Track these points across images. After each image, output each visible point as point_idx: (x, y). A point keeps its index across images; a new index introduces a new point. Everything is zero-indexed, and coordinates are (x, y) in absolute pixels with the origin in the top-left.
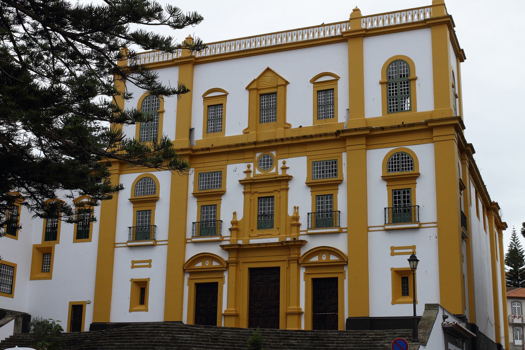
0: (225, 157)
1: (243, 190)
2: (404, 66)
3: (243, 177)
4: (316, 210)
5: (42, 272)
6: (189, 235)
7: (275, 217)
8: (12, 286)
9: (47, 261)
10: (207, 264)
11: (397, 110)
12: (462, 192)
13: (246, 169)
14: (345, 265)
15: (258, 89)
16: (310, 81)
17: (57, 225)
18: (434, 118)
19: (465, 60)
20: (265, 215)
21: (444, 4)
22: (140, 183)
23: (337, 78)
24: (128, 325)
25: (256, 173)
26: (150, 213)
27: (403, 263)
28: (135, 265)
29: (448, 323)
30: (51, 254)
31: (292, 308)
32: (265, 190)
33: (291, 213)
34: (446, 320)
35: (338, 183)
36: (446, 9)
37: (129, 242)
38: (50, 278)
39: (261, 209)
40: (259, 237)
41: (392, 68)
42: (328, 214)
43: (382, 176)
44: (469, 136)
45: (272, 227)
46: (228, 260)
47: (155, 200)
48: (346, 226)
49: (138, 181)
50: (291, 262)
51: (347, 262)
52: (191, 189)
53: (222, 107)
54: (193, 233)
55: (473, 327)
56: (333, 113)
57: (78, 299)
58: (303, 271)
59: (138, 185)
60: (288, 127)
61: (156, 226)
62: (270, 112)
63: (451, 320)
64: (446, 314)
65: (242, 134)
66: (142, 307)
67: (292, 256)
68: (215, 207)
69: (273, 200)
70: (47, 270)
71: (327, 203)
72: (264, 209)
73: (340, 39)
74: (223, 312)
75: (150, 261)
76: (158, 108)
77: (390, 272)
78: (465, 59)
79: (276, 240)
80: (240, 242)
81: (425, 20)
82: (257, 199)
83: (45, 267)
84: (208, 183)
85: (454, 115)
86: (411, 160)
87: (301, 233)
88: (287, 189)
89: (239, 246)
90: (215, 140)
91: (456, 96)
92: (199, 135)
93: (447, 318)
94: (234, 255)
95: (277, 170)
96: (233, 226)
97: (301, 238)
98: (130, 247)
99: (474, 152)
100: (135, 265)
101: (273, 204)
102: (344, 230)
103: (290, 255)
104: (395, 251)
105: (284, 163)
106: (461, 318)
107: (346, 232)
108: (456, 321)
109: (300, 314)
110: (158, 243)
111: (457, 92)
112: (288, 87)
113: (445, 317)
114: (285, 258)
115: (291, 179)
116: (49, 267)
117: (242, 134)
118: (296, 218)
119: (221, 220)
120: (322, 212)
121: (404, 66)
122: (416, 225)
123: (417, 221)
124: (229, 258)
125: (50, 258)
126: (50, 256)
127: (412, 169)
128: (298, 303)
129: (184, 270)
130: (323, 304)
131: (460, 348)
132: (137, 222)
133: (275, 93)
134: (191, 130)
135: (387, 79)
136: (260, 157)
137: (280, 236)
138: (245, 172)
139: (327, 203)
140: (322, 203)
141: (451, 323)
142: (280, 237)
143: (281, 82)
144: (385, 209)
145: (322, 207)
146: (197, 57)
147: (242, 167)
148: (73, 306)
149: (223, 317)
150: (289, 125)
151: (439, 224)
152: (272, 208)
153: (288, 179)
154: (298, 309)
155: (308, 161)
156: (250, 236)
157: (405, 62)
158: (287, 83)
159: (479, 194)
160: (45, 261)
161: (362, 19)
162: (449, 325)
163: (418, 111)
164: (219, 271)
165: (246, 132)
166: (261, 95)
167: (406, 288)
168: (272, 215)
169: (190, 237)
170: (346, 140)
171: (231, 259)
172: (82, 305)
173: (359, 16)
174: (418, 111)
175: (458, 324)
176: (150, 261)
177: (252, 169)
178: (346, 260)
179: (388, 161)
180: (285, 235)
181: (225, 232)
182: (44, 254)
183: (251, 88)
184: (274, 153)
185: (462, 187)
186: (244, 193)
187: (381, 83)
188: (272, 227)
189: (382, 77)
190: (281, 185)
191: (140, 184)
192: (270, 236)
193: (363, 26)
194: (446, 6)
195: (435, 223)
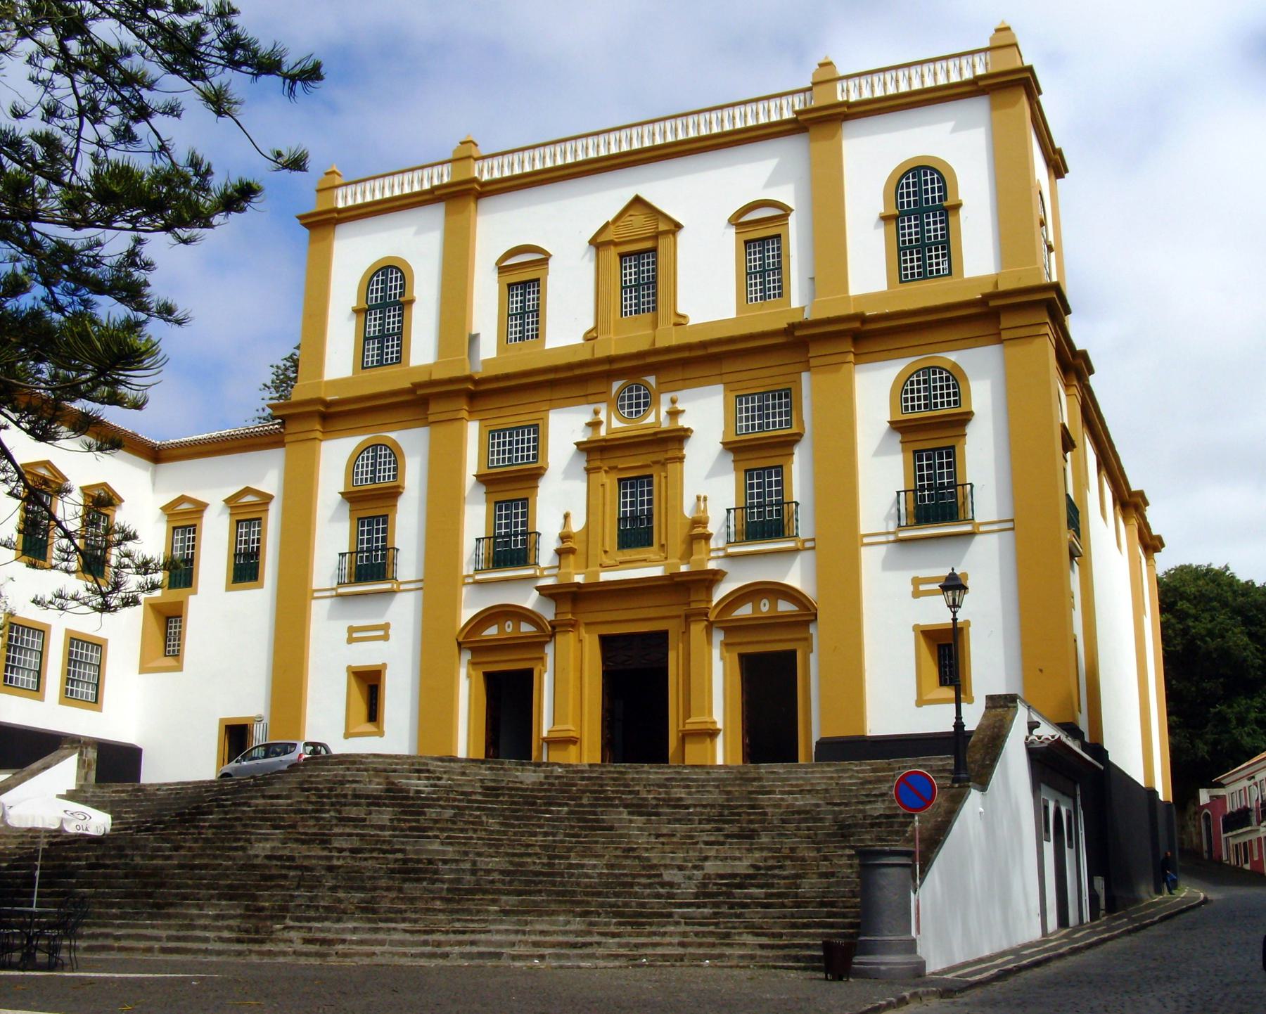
0: (546, 395)
1: (585, 465)
2: (932, 180)
3: (582, 438)
5: (165, 656)
6: (467, 568)
8: (97, 685)
9: (175, 633)
10: (509, 627)
11: (919, 274)
12: (1069, 454)
13: (588, 418)
14: (812, 621)
16: (730, 221)
17: (258, 547)
18: (1001, 288)
19: (1066, 175)
21: (1015, 45)
22: (363, 458)
23: (786, 211)
24: (354, 763)
25: (613, 426)
26: (385, 522)
27: (936, 612)
28: (355, 635)
29: (1039, 738)
30: (181, 616)
31: (695, 721)
32: (632, 463)
33: (688, 510)
34: (1036, 732)
35: (789, 443)
36: (1021, 57)
38: (179, 668)
39: (625, 506)
40: (621, 566)
41: (908, 184)
44: (1081, 333)
45: (650, 544)
46: (553, 618)
50: (692, 619)
52: (472, 464)
53: (538, 286)
54: (477, 562)
55: (1099, 751)
56: (780, 288)
58: (718, 637)
59: (905, 391)
60: (680, 322)
61: (398, 550)
63: (1047, 731)
64: (1036, 718)
65: (582, 342)
67: (694, 606)
68: (525, 503)
69: (650, 484)
70: (174, 651)
74: (545, 734)
75: (386, 627)
78: (1067, 171)
79: (656, 571)
81: (977, 79)
83: (170, 646)
84: (510, 451)
85: (1046, 280)
87: (713, 555)
88: (681, 459)
89: (578, 587)
90: (525, 358)
91: (1050, 249)
92: (488, 349)
93: (1038, 727)
94: (567, 607)
95: (656, 418)
96: (563, 542)
97: (712, 565)
98: (477, 583)
99: (1091, 371)
100: (355, 635)
101: (650, 493)
103: (689, 604)
104: (922, 588)
106: (1071, 729)
107: (813, 548)
108: (1058, 734)
109: (713, 734)
111: (1051, 239)
113: (1032, 726)
114: (681, 610)
115: (688, 437)
116: (179, 645)
117: (582, 342)
118: (700, 522)
121: (932, 180)
122: (968, 528)
124: (556, 614)
125: (180, 627)
126: (181, 621)
129: (459, 644)
131: (1069, 796)
133: (654, 250)
134: (474, 339)
135: (897, 208)
136: (621, 390)
137: (667, 562)
138: (589, 425)
141: (1047, 739)
142: (668, 564)
143: (663, 227)
144: (898, 493)
146: (483, 180)
148: (227, 727)
149: (545, 745)
150: (684, 317)
152: (650, 502)
153: (681, 436)
156: (601, 565)
157: (934, 170)
158: (678, 226)
159: (1103, 472)
160: (170, 633)
161: (839, 86)
162: (1042, 742)
163: (966, 276)
164: (535, 645)
165: (589, 337)
167: (947, 670)
169: (471, 572)
170: (808, 345)
171: (560, 617)
173: (833, 77)
174: (966, 276)
175: (1064, 739)
176: (386, 627)
177: (603, 416)
178: (814, 611)
182: (168, 618)
183: (599, 240)
184: (651, 380)
185: (1068, 444)
186: (588, 471)
188: (650, 544)
190: (667, 451)
191: (363, 460)
192: (644, 564)
193: (840, 98)
194: (1020, 48)
195: (813, 540)
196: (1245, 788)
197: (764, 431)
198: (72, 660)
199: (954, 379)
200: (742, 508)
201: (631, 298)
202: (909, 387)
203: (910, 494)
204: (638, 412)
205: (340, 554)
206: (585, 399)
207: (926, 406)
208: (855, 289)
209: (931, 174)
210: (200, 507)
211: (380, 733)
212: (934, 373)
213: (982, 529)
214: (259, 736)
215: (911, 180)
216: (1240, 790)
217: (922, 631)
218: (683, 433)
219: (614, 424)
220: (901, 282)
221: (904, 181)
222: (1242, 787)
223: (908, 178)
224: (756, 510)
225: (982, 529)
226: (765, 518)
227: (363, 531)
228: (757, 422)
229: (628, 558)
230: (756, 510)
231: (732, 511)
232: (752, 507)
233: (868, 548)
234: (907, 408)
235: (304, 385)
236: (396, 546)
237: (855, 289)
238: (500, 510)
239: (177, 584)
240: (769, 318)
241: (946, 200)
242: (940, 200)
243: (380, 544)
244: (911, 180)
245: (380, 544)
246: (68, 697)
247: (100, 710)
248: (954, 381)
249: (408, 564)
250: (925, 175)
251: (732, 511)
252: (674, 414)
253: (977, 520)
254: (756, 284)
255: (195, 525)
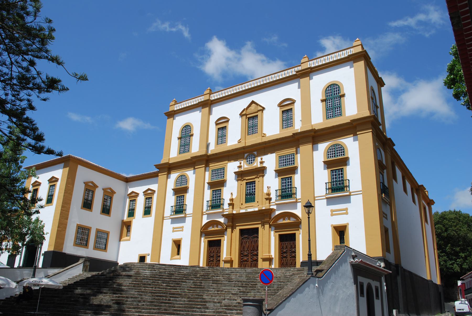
2: (336, 88)
3: (237, 170)
4: (212, 199)
7: (256, 195)
11: (332, 116)
13: (239, 165)
15: (246, 115)
17: (151, 205)
20: (250, 194)
23: (293, 102)
25: (245, 167)
30: (130, 225)
31: (266, 255)
33: (265, 191)
37: (171, 215)
42: (340, 183)
43: (323, 161)
45: (254, 201)
47: (345, 161)
48: (300, 198)
49: (329, 148)
51: (301, 222)
57: (143, 253)
59: (329, 152)
60: (264, 135)
61: (186, 205)
62: (254, 127)
66: (178, 257)
69: (255, 184)
71: (288, 182)
72: (250, 190)
73: (347, 59)
76: (190, 133)
77: (331, 228)
80: (234, 212)
82: (245, 184)
86: (343, 149)
89: (233, 215)
90: (222, 148)
95: (257, 164)
100: (175, 230)
101: (255, 186)
102: (299, 200)
104: (334, 213)
105: (262, 159)
110: (187, 216)
112: (264, 112)
118: (269, 194)
119: (348, 180)
120: (336, 181)
122: (348, 194)
123: (348, 190)
126: (130, 227)
127: (343, 154)
128: (269, 252)
130: (248, 255)
132: (281, 186)
135: (326, 97)
139: (288, 182)
140: (336, 175)
145: (336, 178)
147: (237, 163)
151: (364, 192)
152: (255, 189)
154: (270, 256)
155: (276, 156)
156: (240, 208)
157: (336, 85)
163: (346, 116)
164: (222, 233)
165: (239, 142)
166: (249, 118)
168: (254, 194)
172: (145, 256)
178: (300, 221)
179: (328, 151)
180: (262, 206)
181: (226, 206)
187: (322, 101)
188: (254, 201)
189: (322, 96)
192: (252, 207)
196: (470, 281)
197: (287, 166)
198: (97, 237)
199: (343, 147)
200: (330, 182)
201: (251, 130)
202: (329, 151)
203: (175, 207)
204: (252, 163)
205: (207, 201)
206: (236, 160)
207: (334, 156)
208: (314, 122)
209: (336, 86)
210: (137, 195)
211: (180, 259)
212: (337, 146)
213: (352, 194)
214: (148, 260)
215: (330, 89)
216: (469, 281)
217: (334, 227)
218: (263, 168)
219: (245, 166)
220: (327, 119)
221: (328, 89)
222: (469, 280)
223: (329, 88)
224: (335, 183)
225: (352, 194)
226: (338, 185)
227: (214, 194)
228: (292, 162)
229: (248, 206)
230: (335, 183)
231: (327, 183)
232: (333, 182)
233: (191, 213)
234: (328, 157)
235: (164, 159)
236: (186, 204)
237: (314, 122)
238: (214, 193)
239: (147, 214)
240: (288, 132)
241: (340, 93)
242: (339, 94)
243: (178, 204)
244: (330, 89)
245: (178, 204)
246: (96, 248)
247: (106, 252)
248: (341, 149)
249: (189, 209)
250: (334, 86)
251: (327, 183)
252: (262, 163)
253: (351, 191)
254: (285, 123)
255: (152, 197)
